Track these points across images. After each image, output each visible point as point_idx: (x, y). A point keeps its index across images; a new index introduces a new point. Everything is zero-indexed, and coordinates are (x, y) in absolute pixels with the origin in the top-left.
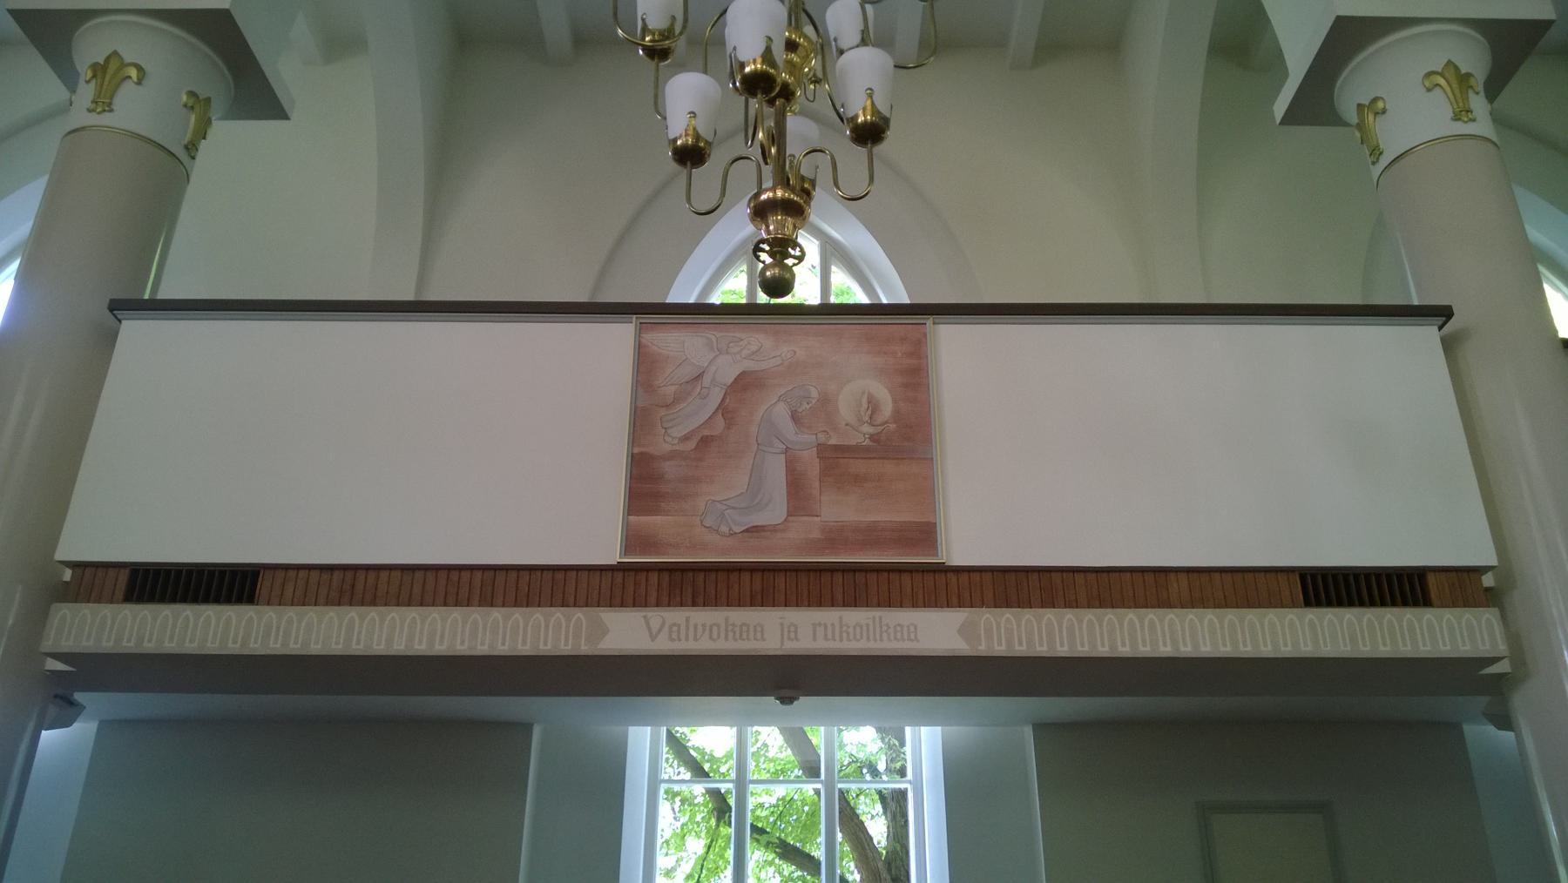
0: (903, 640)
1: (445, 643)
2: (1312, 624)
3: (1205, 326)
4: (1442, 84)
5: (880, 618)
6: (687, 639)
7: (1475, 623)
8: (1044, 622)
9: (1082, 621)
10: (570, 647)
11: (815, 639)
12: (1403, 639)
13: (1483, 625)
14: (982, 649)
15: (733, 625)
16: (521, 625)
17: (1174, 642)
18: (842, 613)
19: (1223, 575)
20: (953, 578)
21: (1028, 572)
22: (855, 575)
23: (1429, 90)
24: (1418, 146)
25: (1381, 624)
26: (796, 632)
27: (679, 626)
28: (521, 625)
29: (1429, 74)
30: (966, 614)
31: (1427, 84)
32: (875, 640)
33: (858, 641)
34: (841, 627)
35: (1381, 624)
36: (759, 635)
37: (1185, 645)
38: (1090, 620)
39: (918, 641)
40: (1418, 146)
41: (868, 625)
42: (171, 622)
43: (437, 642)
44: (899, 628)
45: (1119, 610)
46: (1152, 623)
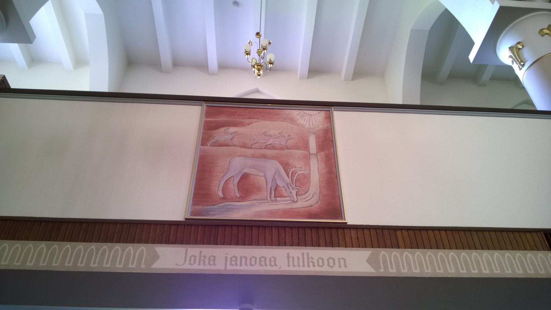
0: (236, 265)
1: (7, 261)
2: (454, 260)
3: (541, 119)
4: (547, 32)
5: (308, 254)
6: (241, 265)
7: (490, 258)
8: (416, 256)
9: (414, 255)
10: (83, 265)
11: (289, 266)
12: (451, 267)
13: (517, 260)
14: (382, 272)
15: (205, 257)
16: (132, 253)
17: (410, 268)
18: (202, 249)
19: (502, 233)
20: (353, 232)
21: (482, 231)
22: (238, 228)
23: (543, 36)
24: (546, 55)
25: (459, 258)
26: (214, 260)
27: (195, 257)
28: (132, 253)
29: (542, 30)
30: (370, 252)
31: (542, 33)
32: (294, 266)
33: (192, 265)
34: (200, 256)
35: (459, 258)
36: (212, 262)
37: (392, 268)
38: (508, 257)
39: (276, 266)
40: (546, 55)
41: (298, 258)
42: (32, 250)
43: (54, 261)
44: (234, 259)
45: (535, 252)
46: (407, 256)
